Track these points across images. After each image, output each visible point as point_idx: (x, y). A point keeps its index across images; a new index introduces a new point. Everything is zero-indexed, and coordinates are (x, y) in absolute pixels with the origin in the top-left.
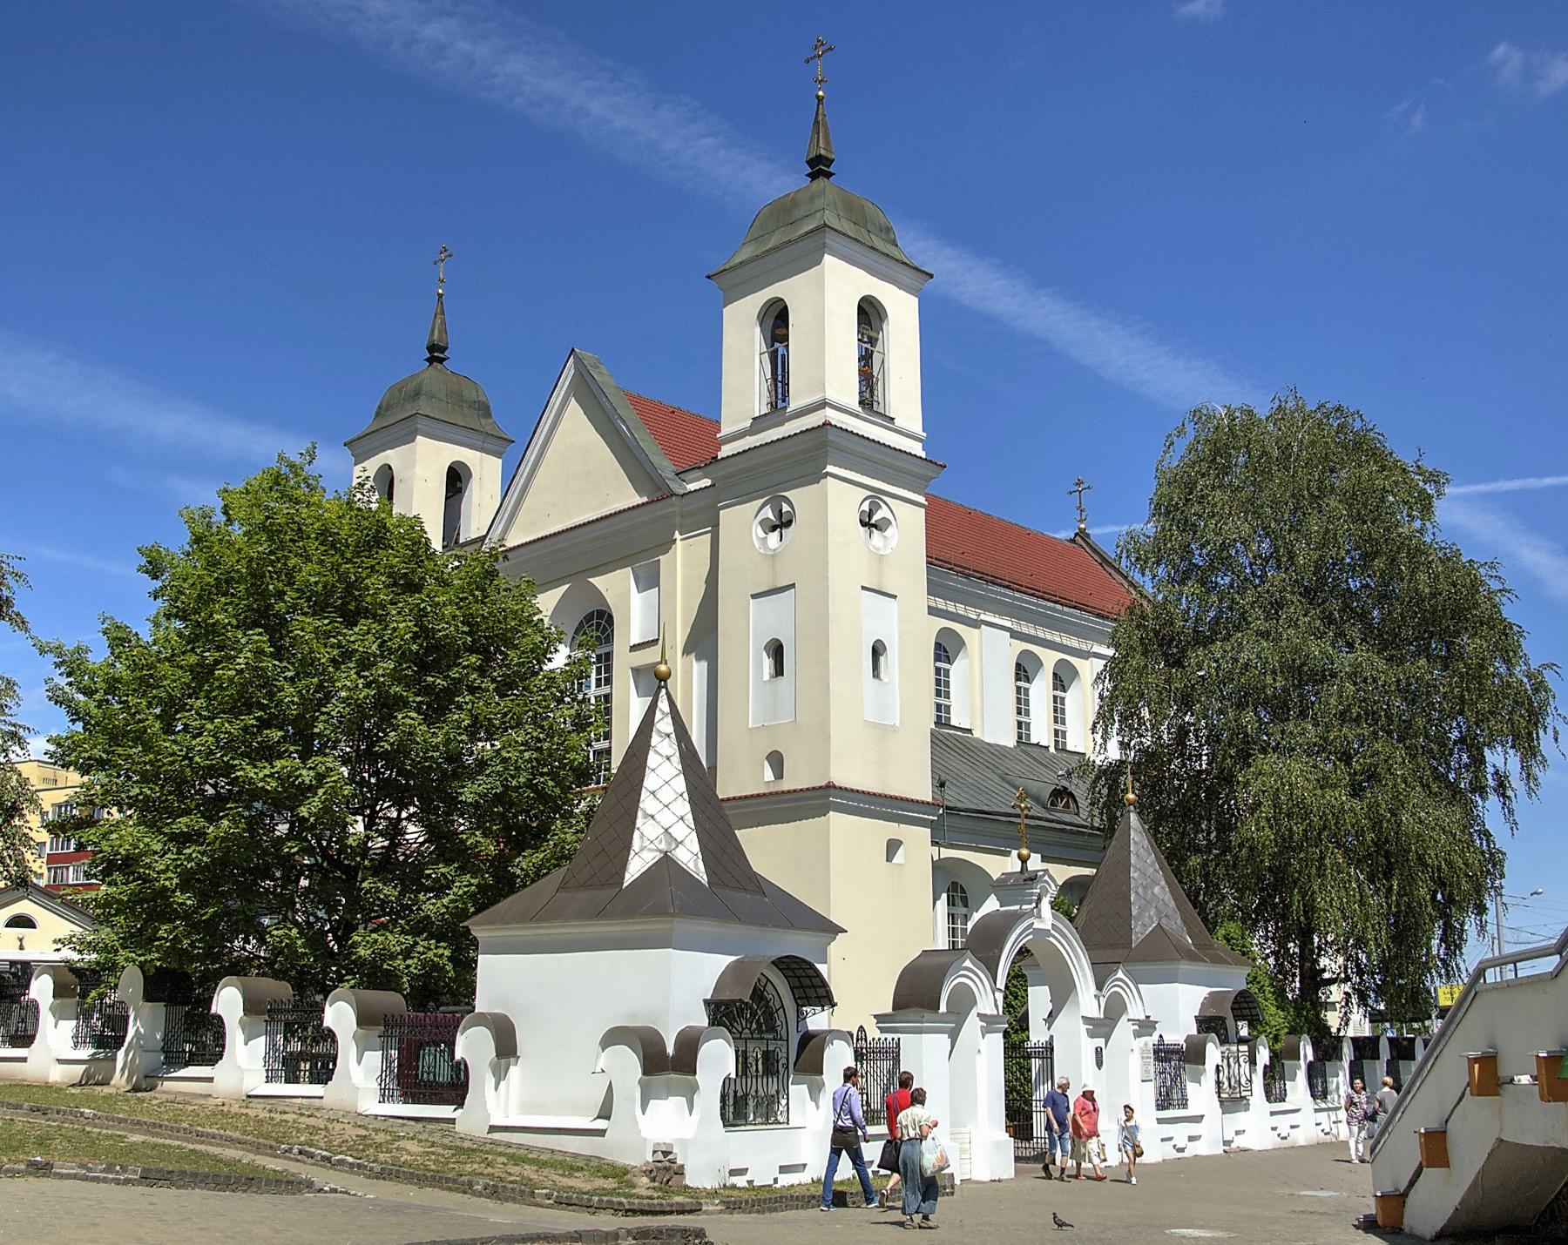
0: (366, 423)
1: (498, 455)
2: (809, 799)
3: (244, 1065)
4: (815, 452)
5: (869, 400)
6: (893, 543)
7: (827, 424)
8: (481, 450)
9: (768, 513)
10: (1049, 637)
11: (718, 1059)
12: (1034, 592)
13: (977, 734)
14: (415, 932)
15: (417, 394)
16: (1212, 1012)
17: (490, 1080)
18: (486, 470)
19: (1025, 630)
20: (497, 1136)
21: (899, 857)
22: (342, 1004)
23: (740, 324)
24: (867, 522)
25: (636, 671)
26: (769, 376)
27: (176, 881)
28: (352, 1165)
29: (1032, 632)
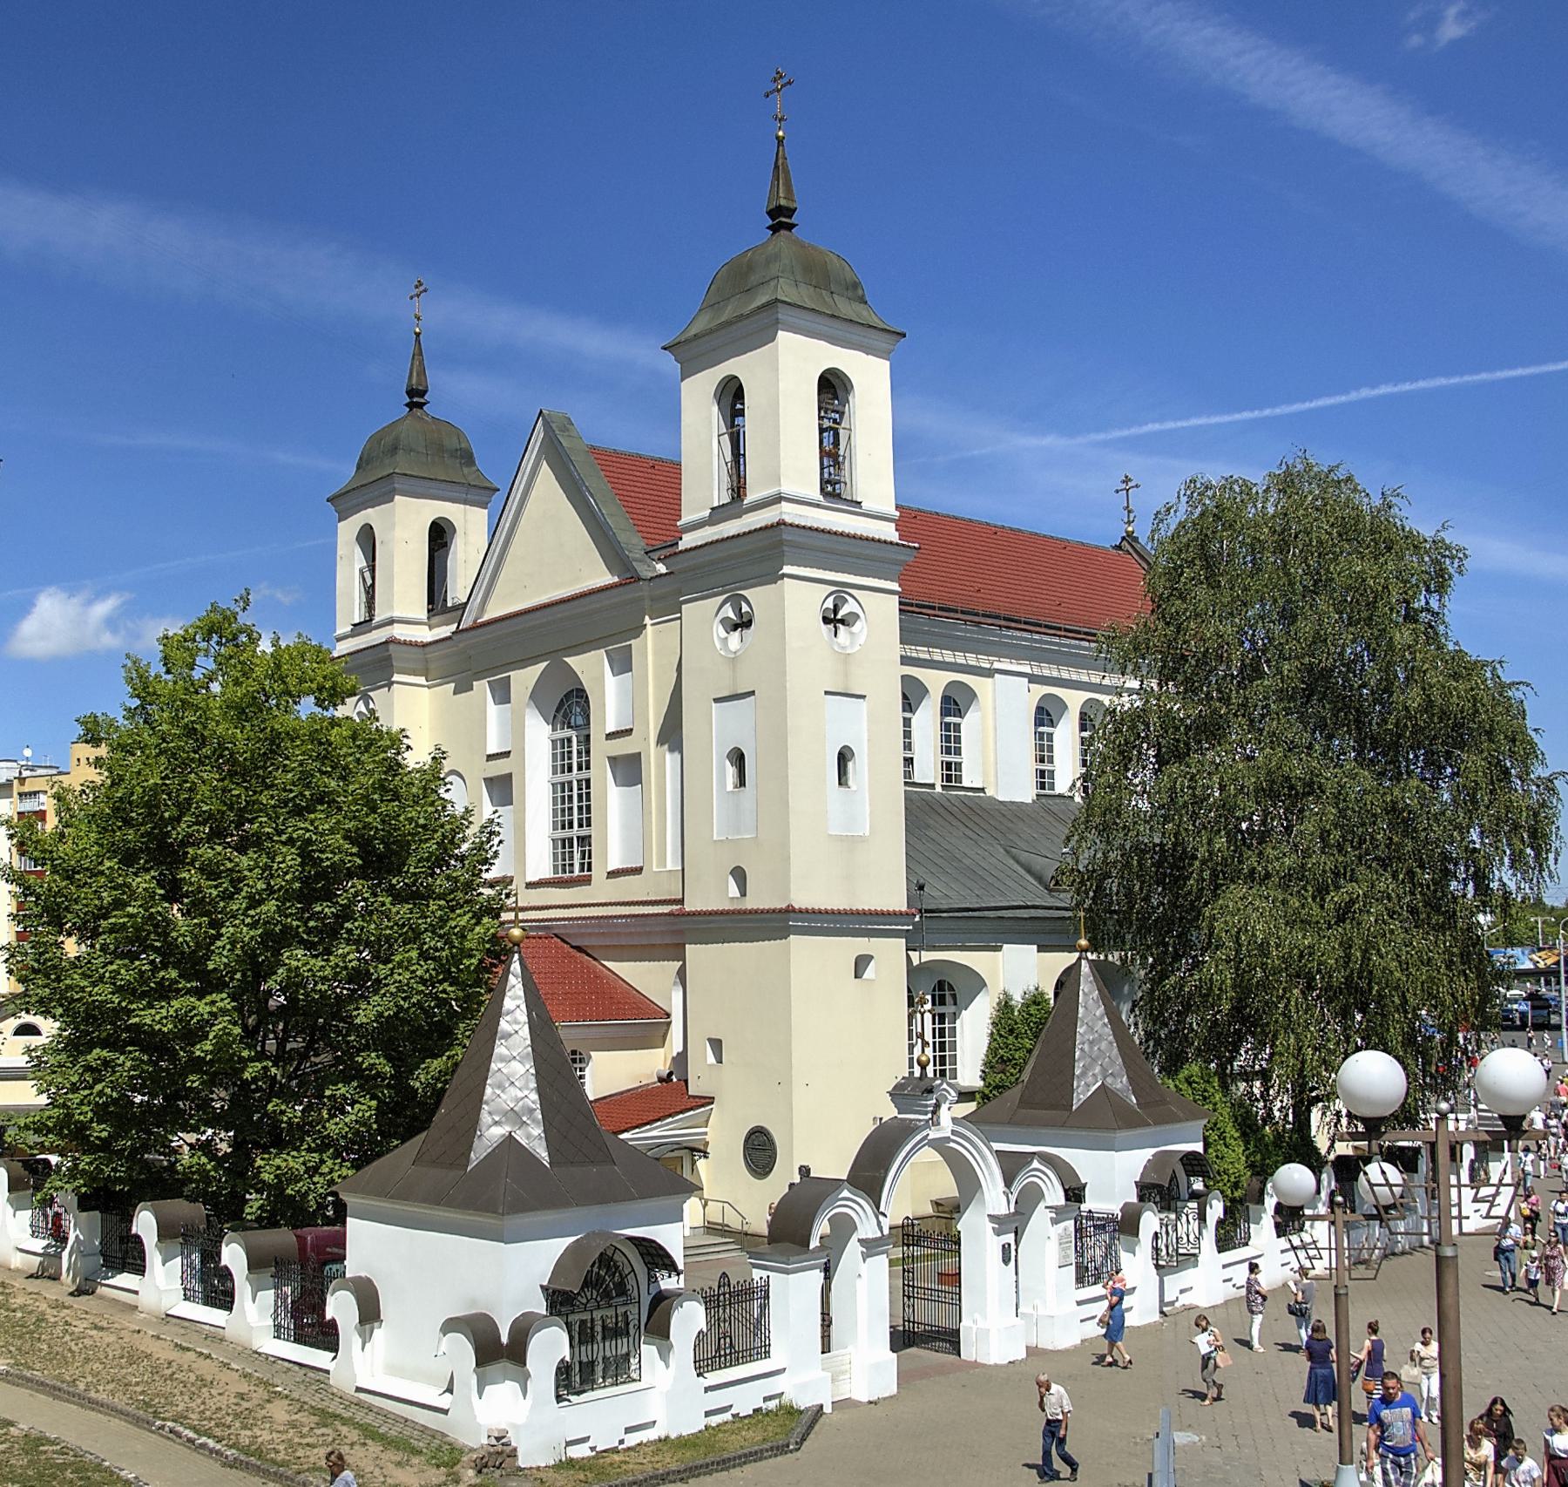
0: (346, 473)
1: (483, 505)
2: (770, 920)
3: (162, 1283)
4: (767, 552)
5: (833, 489)
6: (862, 639)
7: (782, 523)
8: (465, 502)
9: (728, 612)
10: (1074, 677)
11: (551, 1346)
12: (1055, 630)
13: (989, 792)
14: (321, 1149)
15: (394, 449)
16: (1153, 1178)
17: (357, 1341)
18: (471, 524)
19: (1046, 673)
20: (362, 1396)
21: (869, 973)
22: (234, 1245)
23: (697, 398)
24: (832, 619)
25: (613, 760)
26: (729, 458)
27: (90, 1115)
28: (211, 1451)
29: (1055, 674)
